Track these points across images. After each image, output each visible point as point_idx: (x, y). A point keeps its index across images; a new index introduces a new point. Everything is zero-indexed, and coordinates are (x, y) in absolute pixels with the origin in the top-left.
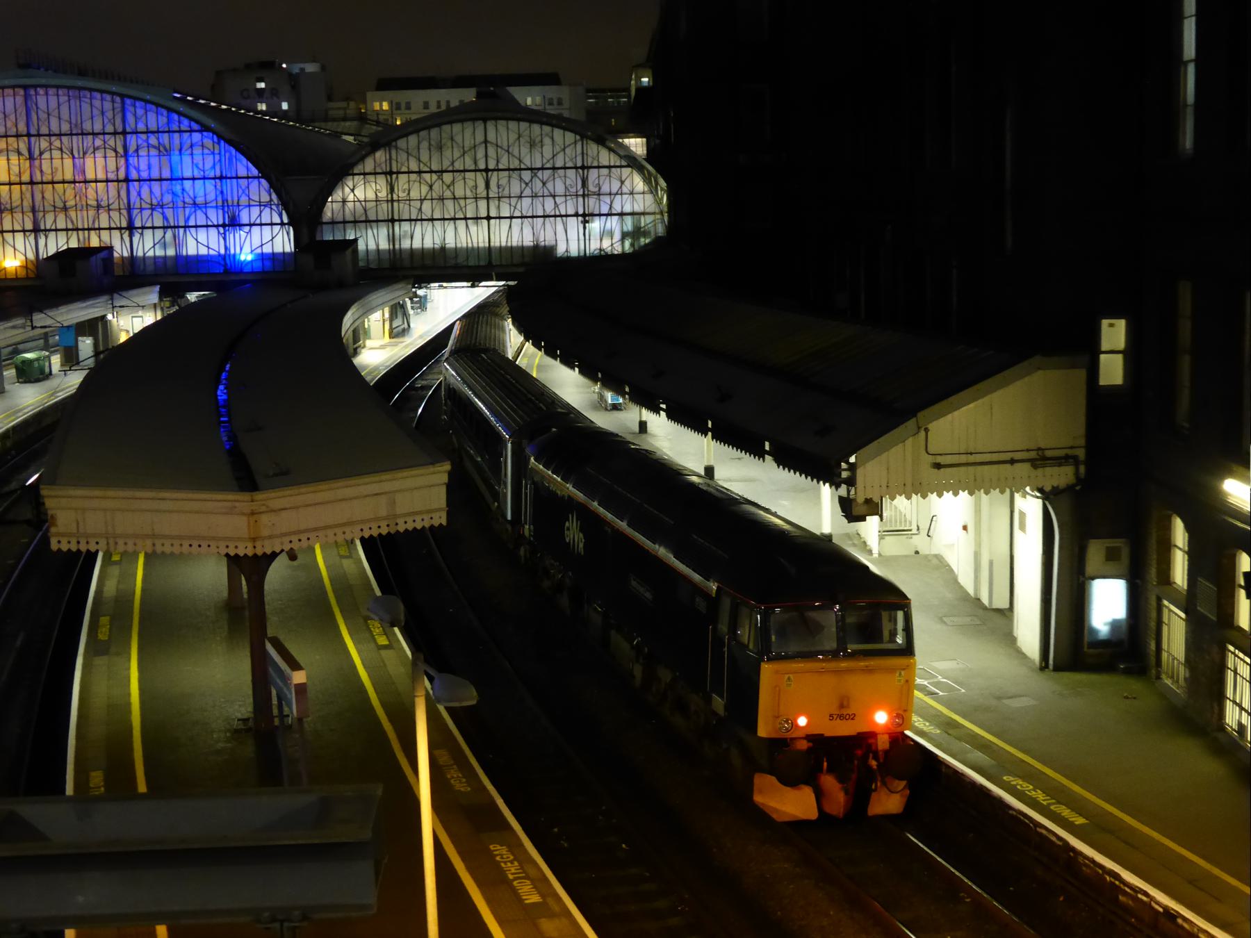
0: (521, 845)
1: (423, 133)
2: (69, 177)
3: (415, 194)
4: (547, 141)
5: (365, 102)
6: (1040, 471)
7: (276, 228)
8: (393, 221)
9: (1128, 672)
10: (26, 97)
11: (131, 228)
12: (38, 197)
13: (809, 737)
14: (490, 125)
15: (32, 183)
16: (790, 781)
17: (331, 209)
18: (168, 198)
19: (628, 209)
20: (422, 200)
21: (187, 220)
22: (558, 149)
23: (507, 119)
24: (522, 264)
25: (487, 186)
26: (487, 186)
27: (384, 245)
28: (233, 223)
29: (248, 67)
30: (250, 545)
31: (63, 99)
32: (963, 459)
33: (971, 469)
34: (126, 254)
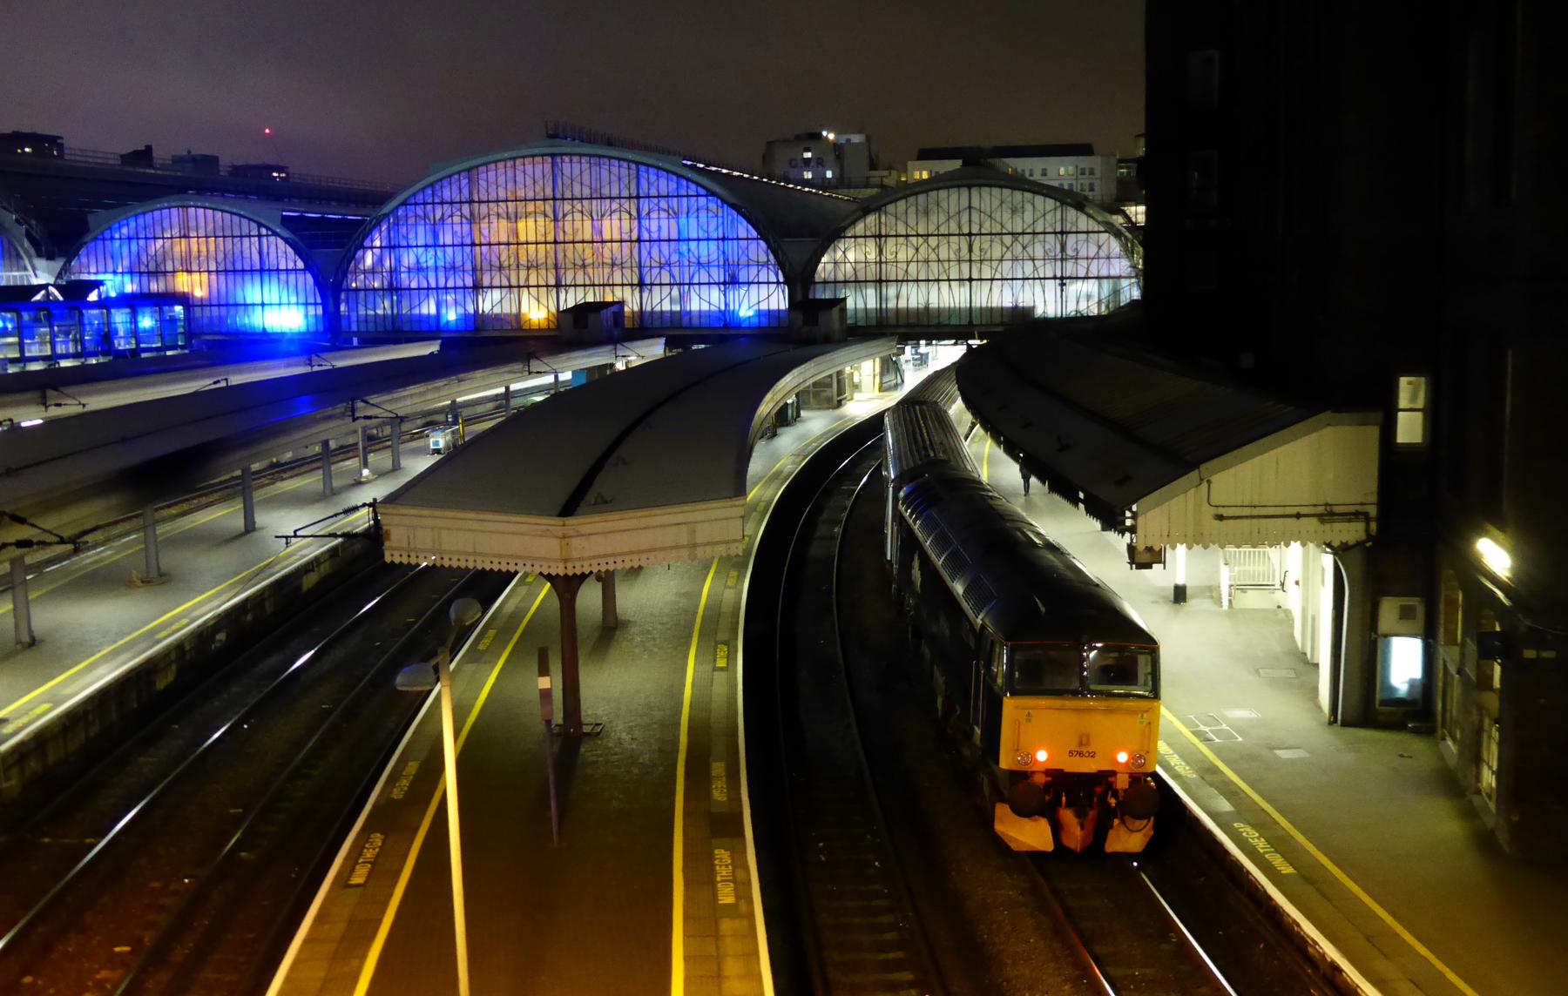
0: (744, 852)
1: (912, 199)
2: (588, 237)
3: (902, 257)
4: (1028, 207)
5: (905, 171)
6: (1327, 526)
7: (773, 287)
8: (880, 281)
9: (1416, 731)
10: (553, 164)
11: (641, 284)
12: (561, 256)
13: (1048, 772)
14: (975, 191)
15: (555, 242)
16: (1023, 811)
17: (825, 267)
18: (675, 258)
19: (1104, 273)
20: (908, 263)
21: (691, 278)
22: (1038, 214)
23: (990, 186)
24: (1002, 324)
25: (970, 250)
26: (970, 250)
27: (872, 304)
28: (732, 282)
29: (798, 137)
30: (561, 566)
31: (586, 166)
32: (1247, 512)
33: (1255, 521)
34: (636, 309)
